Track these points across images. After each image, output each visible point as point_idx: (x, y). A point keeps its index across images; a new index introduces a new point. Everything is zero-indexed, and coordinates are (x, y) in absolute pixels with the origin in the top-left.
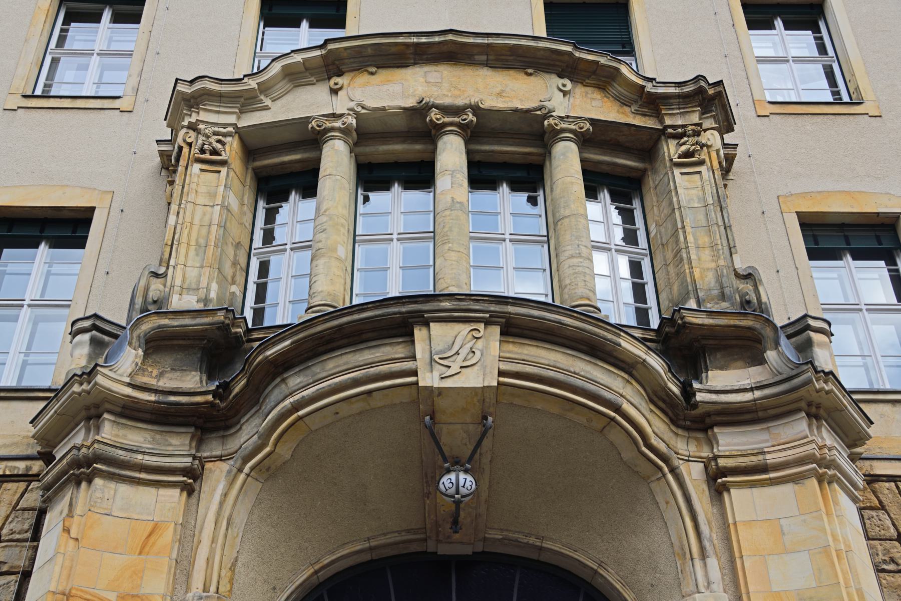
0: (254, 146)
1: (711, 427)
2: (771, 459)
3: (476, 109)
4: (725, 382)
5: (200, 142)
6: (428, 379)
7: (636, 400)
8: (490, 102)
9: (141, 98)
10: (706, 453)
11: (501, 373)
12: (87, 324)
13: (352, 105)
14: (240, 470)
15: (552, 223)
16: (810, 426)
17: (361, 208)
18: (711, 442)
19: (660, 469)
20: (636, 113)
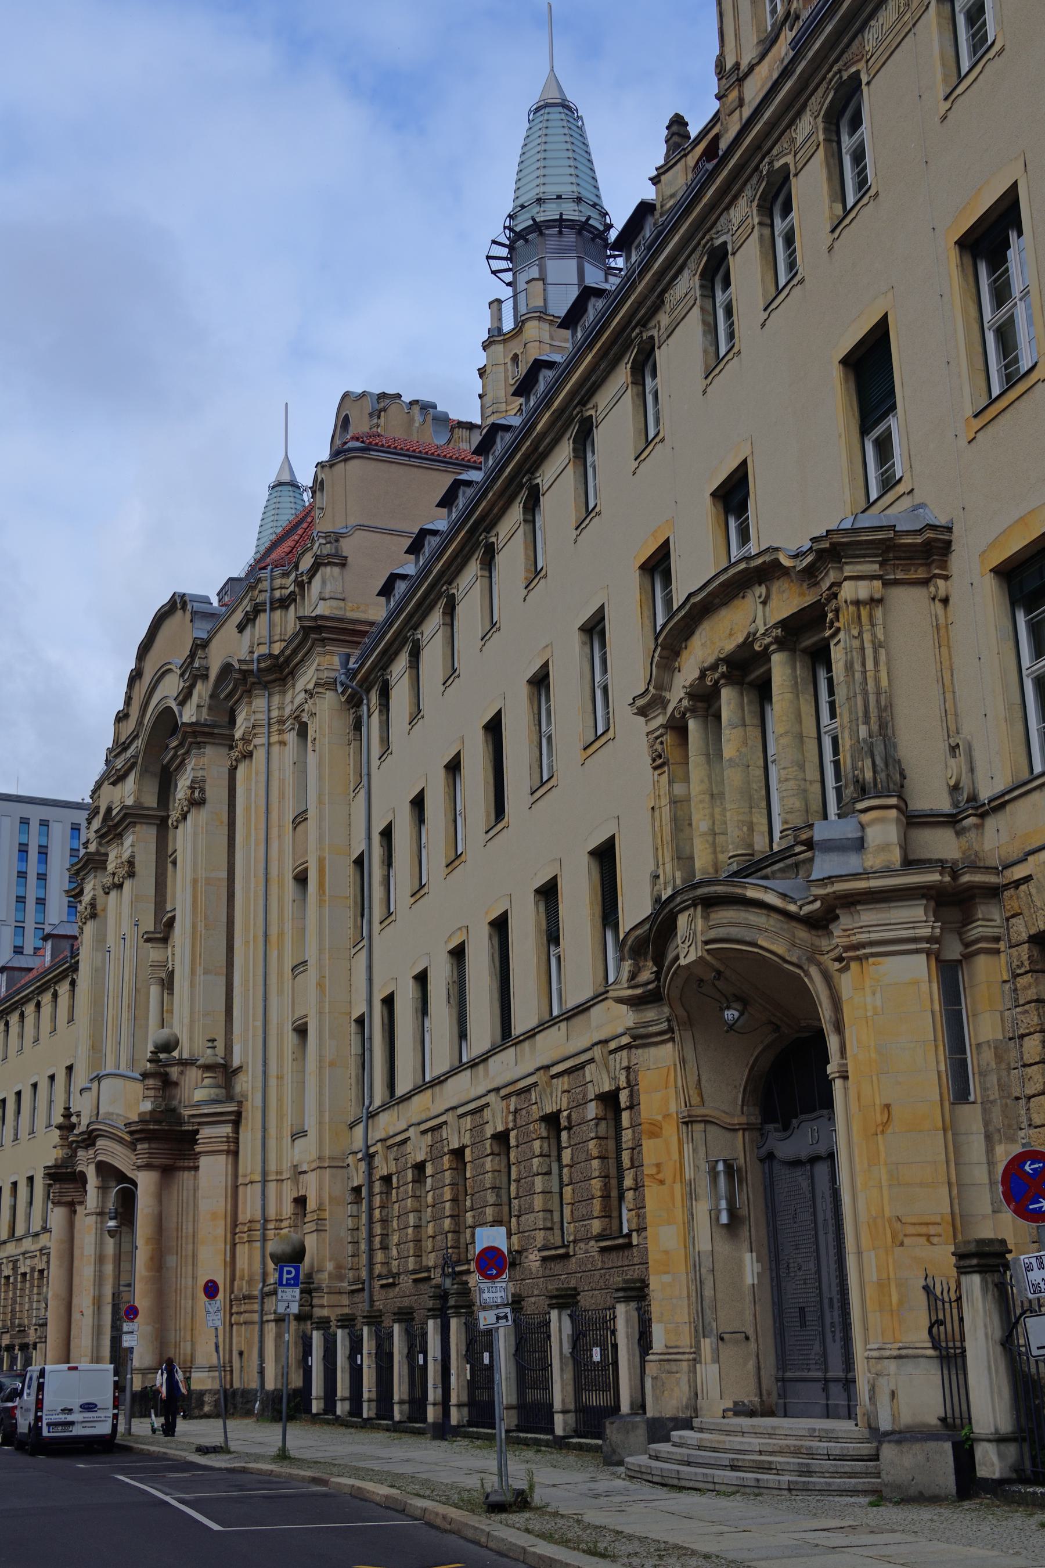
11: (706, 943)
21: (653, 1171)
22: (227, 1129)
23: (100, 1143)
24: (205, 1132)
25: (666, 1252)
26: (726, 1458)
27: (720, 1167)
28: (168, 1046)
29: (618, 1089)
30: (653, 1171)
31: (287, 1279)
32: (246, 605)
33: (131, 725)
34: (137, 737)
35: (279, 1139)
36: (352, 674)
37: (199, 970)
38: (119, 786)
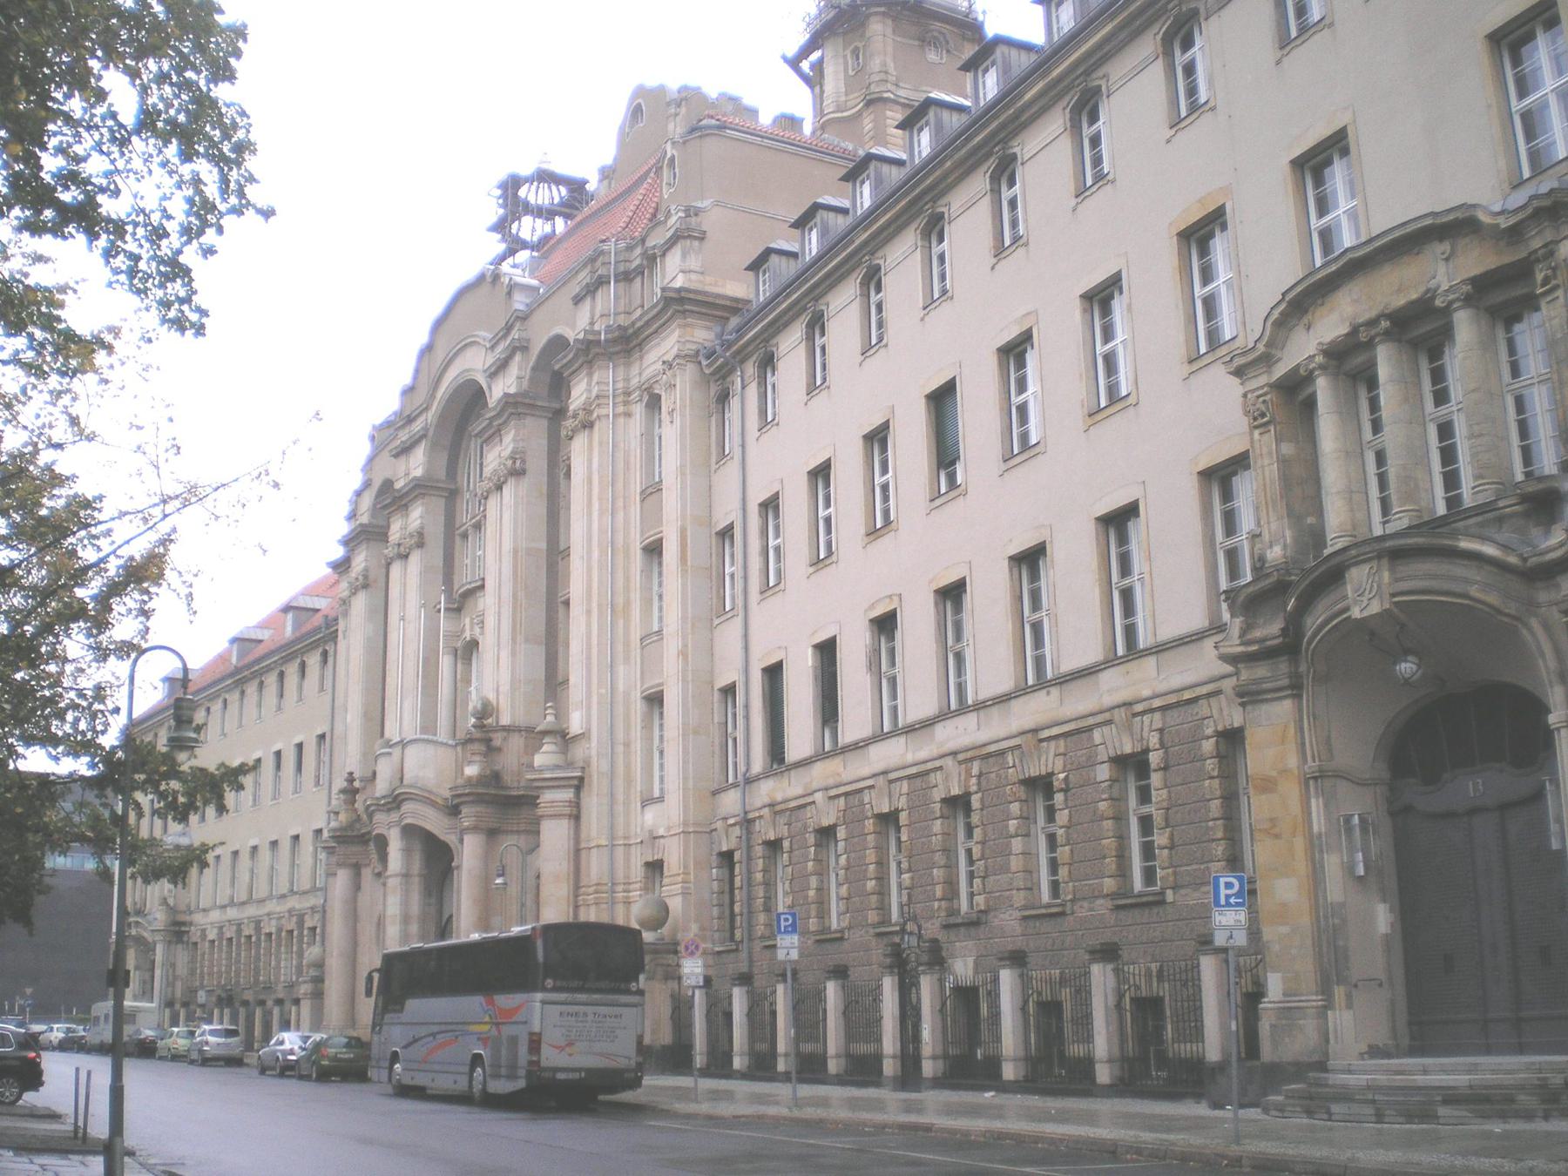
11: (1393, 595)
22: (568, 794)
23: (407, 807)
24: (547, 796)
27: (1356, 820)
28: (486, 711)
29: (1146, 751)
32: (584, 277)
33: (420, 397)
34: (426, 409)
35: (627, 803)
36: (727, 345)
37: (520, 638)
38: (403, 459)
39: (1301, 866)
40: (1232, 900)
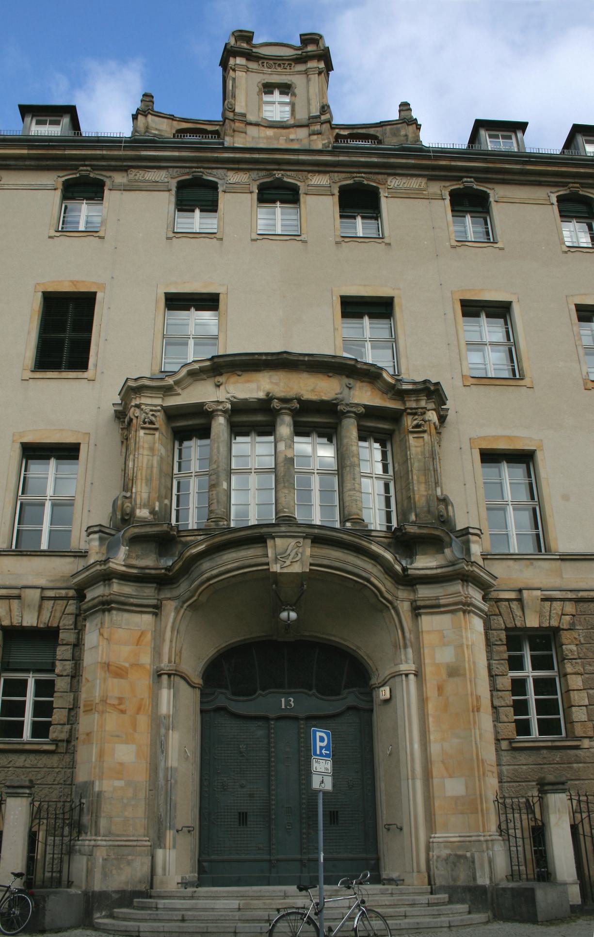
0: (172, 414)
1: (415, 585)
2: (442, 602)
3: (299, 400)
4: (425, 563)
5: (143, 417)
6: (276, 568)
7: (378, 574)
8: (308, 396)
9: (99, 370)
10: (412, 597)
11: (311, 565)
12: (96, 529)
13: (228, 396)
14: (182, 607)
15: (341, 457)
16: (463, 586)
17: (233, 441)
18: (415, 591)
19: (388, 607)
20: (391, 399)
21: (116, 702)
25: (121, 764)
26: (177, 915)
30: (116, 702)
31: (321, 748)
39: (144, 736)
40: (323, 751)
